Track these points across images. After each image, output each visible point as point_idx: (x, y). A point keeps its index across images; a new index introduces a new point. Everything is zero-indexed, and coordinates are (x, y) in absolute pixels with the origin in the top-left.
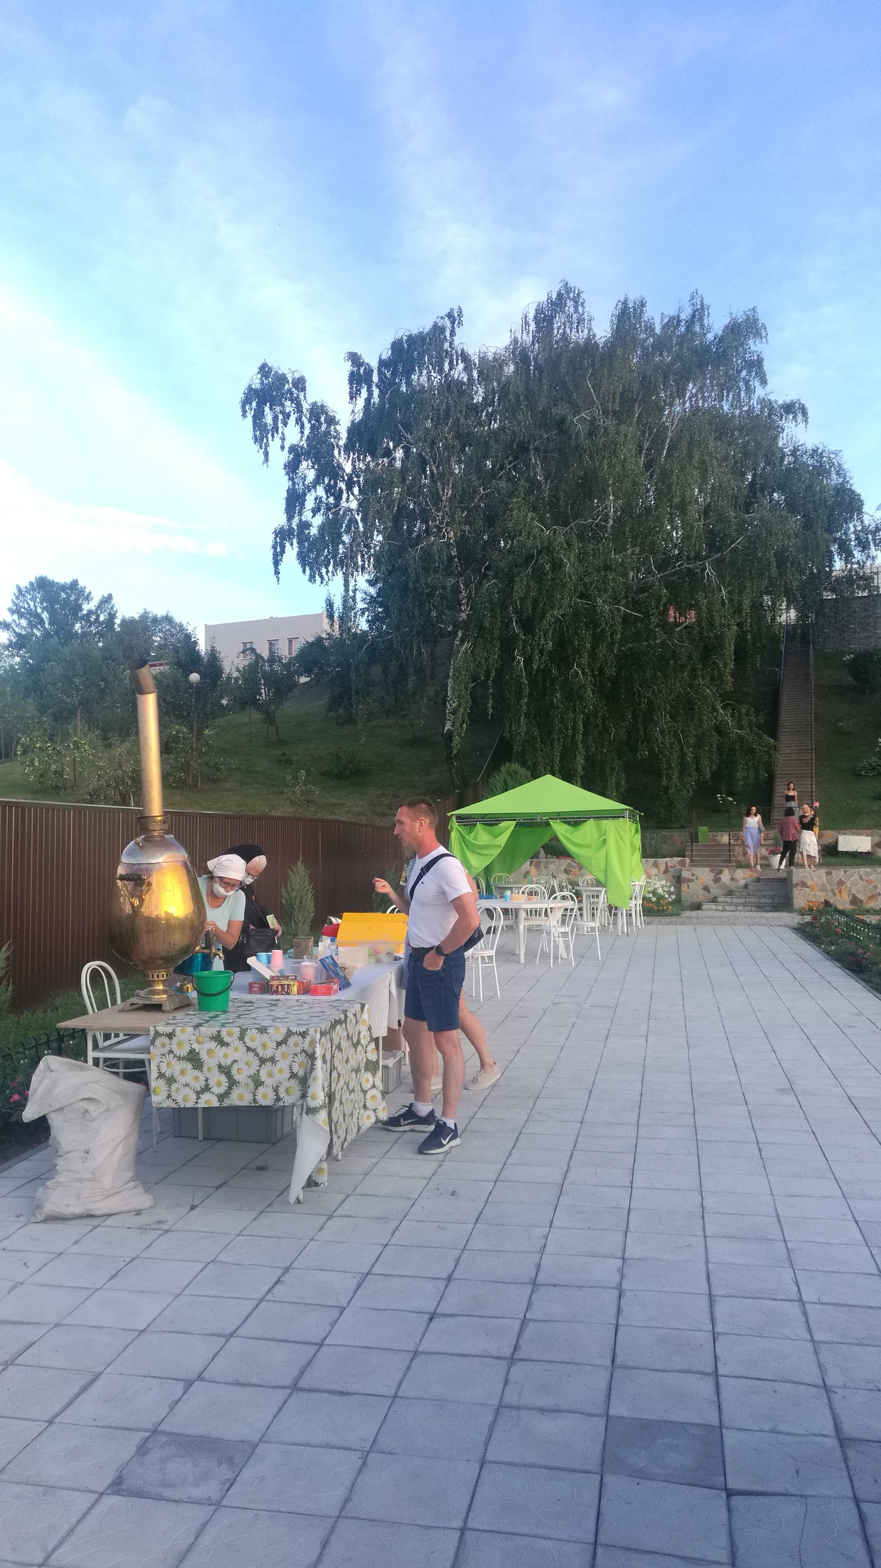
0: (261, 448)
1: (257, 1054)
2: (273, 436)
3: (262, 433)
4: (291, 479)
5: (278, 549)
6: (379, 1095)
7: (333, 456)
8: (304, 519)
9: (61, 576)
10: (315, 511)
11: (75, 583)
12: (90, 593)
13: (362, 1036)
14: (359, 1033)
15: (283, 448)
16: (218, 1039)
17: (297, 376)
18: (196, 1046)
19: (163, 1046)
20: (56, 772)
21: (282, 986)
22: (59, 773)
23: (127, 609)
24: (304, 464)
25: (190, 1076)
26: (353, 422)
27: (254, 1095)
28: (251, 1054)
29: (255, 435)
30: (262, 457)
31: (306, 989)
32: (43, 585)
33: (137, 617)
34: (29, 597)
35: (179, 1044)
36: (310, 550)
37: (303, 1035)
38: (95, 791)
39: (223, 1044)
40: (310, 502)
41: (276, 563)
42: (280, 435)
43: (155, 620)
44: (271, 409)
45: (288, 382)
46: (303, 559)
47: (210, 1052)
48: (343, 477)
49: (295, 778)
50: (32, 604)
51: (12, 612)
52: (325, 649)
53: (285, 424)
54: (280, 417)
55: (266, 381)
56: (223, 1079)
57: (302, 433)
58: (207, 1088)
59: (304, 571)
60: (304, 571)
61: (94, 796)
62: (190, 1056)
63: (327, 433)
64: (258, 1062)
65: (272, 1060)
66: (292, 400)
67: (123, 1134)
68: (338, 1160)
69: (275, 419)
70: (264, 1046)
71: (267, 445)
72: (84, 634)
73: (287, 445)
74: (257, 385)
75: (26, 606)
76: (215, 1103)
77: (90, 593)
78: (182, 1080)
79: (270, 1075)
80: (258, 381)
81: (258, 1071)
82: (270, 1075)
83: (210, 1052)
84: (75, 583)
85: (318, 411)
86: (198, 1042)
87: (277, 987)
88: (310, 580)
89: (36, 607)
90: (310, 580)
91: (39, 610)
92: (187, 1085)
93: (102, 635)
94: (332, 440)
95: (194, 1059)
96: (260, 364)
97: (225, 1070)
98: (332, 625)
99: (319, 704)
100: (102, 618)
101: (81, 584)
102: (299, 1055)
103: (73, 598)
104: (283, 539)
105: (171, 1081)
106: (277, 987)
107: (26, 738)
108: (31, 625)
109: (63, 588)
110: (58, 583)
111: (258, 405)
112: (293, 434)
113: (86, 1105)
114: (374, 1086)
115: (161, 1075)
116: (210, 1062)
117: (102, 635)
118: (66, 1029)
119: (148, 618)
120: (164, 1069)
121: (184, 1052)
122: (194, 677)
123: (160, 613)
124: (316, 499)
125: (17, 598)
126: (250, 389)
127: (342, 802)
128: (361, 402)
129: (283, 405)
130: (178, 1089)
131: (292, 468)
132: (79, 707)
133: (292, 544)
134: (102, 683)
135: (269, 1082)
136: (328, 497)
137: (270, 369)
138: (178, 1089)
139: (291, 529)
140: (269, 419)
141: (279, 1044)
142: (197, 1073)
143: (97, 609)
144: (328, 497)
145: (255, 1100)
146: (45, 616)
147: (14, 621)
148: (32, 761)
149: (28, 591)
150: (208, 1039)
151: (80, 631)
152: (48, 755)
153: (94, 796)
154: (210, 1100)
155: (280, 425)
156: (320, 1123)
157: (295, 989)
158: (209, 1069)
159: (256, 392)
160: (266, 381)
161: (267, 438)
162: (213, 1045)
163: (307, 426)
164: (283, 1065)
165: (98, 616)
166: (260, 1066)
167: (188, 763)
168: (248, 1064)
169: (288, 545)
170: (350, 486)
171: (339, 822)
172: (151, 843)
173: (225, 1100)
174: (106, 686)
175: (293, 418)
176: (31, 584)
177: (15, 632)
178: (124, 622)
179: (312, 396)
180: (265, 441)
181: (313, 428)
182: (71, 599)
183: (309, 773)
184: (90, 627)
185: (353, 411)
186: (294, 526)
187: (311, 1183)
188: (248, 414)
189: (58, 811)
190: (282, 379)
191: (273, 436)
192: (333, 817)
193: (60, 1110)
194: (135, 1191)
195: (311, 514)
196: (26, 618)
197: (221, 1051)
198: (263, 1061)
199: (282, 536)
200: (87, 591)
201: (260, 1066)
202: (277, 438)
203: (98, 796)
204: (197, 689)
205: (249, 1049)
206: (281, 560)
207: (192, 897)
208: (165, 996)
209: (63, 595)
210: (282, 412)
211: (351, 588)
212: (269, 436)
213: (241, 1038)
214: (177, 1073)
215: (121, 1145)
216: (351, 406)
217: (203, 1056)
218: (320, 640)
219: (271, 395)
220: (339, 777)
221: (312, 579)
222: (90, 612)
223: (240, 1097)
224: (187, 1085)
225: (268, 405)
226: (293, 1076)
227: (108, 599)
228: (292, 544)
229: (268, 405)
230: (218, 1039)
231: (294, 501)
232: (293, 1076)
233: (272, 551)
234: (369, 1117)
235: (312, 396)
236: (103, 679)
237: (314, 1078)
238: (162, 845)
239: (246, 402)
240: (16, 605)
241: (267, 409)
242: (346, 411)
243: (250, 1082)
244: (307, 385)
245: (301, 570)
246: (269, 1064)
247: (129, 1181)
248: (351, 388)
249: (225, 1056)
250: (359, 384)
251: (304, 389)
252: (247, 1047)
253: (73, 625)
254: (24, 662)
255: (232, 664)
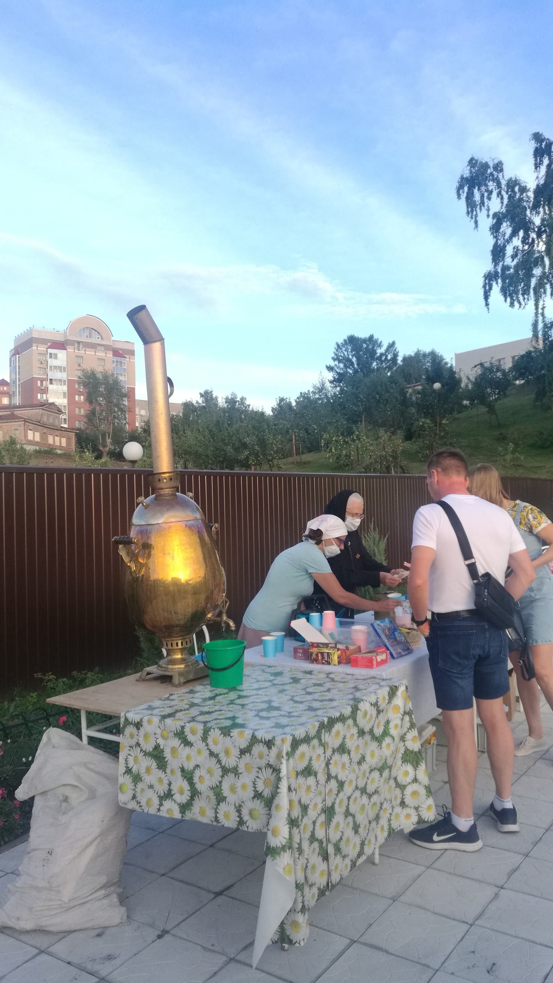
0: (472, 218)
1: (219, 761)
2: (481, 209)
3: (472, 206)
4: (495, 237)
5: (487, 288)
6: (423, 792)
7: (525, 215)
8: (505, 264)
9: (362, 334)
10: (513, 257)
11: (371, 337)
12: (381, 342)
13: (392, 725)
14: (388, 722)
15: (488, 216)
16: (180, 735)
17: (496, 161)
18: (161, 741)
19: (132, 736)
20: (346, 455)
21: (322, 654)
22: (348, 456)
23: (405, 350)
24: (504, 224)
25: (153, 776)
26: (538, 185)
27: (216, 813)
28: (214, 760)
29: (468, 210)
30: (473, 224)
31: (347, 659)
32: (352, 340)
33: (413, 354)
34: (344, 349)
35: (146, 736)
36: (510, 285)
37: (269, 744)
38: (367, 466)
39: (187, 743)
40: (509, 250)
41: (486, 297)
42: (486, 207)
43: (425, 355)
44: (479, 189)
45: (490, 167)
46: (504, 291)
47: (174, 750)
48: (534, 229)
49: (506, 449)
50: (346, 353)
51: (334, 359)
52: (532, 359)
53: (489, 199)
54: (486, 194)
55: (474, 171)
56: (186, 786)
57: (502, 203)
58: (169, 795)
59: (506, 301)
60: (506, 301)
61: (367, 469)
62: (155, 753)
63: (521, 200)
64: (219, 772)
65: (235, 771)
66: (493, 180)
67: (96, 831)
68: (374, 864)
69: (482, 196)
70: (227, 753)
71: (476, 216)
72: (378, 369)
73: (491, 213)
74: (467, 174)
75: (343, 355)
76: (177, 815)
77: (381, 342)
78: (148, 779)
79: (233, 789)
80: (468, 171)
81: (220, 782)
82: (233, 789)
83: (174, 750)
84: (371, 337)
85: (513, 184)
86: (163, 737)
87: (317, 655)
88: (510, 306)
89: (348, 355)
90: (510, 306)
91: (350, 357)
92: (151, 787)
93: (390, 368)
94: (525, 204)
95: (157, 755)
96: (468, 159)
97: (188, 775)
98: (537, 341)
99: (528, 398)
100: (389, 357)
101: (375, 337)
102: (263, 770)
103: (370, 347)
104: (490, 280)
105: (137, 779)
106: (317, 655)
107: (326, 435)
108: (346, 366)
109: (364, 341)
110: (361, 338)
111: (469, 189)
112: (496, 205)
113: (67, 791)
114: (415, 780)
115: (128, 771)
116: (173, 763)
117: (390, 368)
118: (54, 706)
119: (420, 354)
120: (131, 764)
121: (149, 747)
122: (437, 386)
123: (428, 350)
124: (514, 248)
125: (337, 350)
126: (462, 178)
127: (544, 465)
128: (543, 169)
129: (486, 185)
130: (143, 790)
131: (495, 229)
132: (362, 413)
133: (497, 283)
134: (377, 396)
135: (231, 798)
136: (524, 246)
137: (477, 161)
138: (143, 790)
139: (496, 273)
140: (477, 196)
141: (243, 752)
142: (160, 774)
143: (386, 352)
144: (524, 246)
145: (216, 819)
146: (354, 360)
147: (336, 365)
148: (331, 450)
149: (343, 345)
150: (172, 734)
151: (376, 368)
152: (340, 445)
153: (367, 469)
154: (171, 810)
155: (486, 200)
156: (281, 871)
157: (335, 658)
158: (172, 771)
159: (467, 179)
160: (474, 171)
161: (476, 211)
162: (176, 742)
163: (506, 197)
164: (246, 779)
165: (387, 356)
166: (222, 777)
167: (432, 445)
168: (209, 772)
169: (494, 284)
170: (539, 235)
171: (541, 480)
172: (163, 503)
173: (187, 813)
174: (380, 397)
175: (494, 195)
176: (345, 341)
177: (337, 372)
178: (405, 359)
179: (508, 173)
180: (474, 213)
181: (510, 197)
182: (370, 347)
183: (517, 445)
184: (382, 363)
185: (537, 177)
186: (499, 270)
187: (283, 939)
188: (461, 196)
189: (356, 478)
190: (486, 166)
191: (481, 209)
192: (536, 476)
193: (43, 793)
194: (105, 901)
195: (511, 260)
196: (343, 363)
197: (185, 751)
198: (225, 771)
199: (490, 278)
200: (379, 341)
201: (222, 777)
202: (484, 210)
203: (370, 470)
204: (438, 394)
205: (212, 754)
206: (489, 295)
207: (205, 558)
208: (182, 666)
209: (365, 346)
210: (487, 191)
211: (540, 307)
212: (478, 209)
213: (204, 739)
214: (143, 771)
215: (95, 844)
216: (536, 175)
217: (167, 754)
218: (529, 353)
219: (478, 178)
220: (542, 447)
221: (512, 305)
222: (382, 355)
223: (202, 813)
224: (151, 787)
225: (477, 188)
226: (258, 795)
227: (392, 345)
228: (497, 283)
229: (477, 188)
230: (180, 735)
231: (498, 253)
232: (258, 795)
233: (483, 289)
234: (408, 816)
235: (508, 173)
236: (378, 393)
237: (277, 807)
238: (172, 503)
239: (460, 188)
240: (336, 355)
241: (476, 191)
242: (531, 177)
243: (211, 794)
244: (504, 166)
245: (504, 299)
246: (231, 775)
247: (101, 888)
248: (536, 160)
249: (188, 758)
250: (542, 156)
251: (502, 170)
252: (210, 750)
253: (372, 363)
254: (342, 390)
255: (468, 375)
